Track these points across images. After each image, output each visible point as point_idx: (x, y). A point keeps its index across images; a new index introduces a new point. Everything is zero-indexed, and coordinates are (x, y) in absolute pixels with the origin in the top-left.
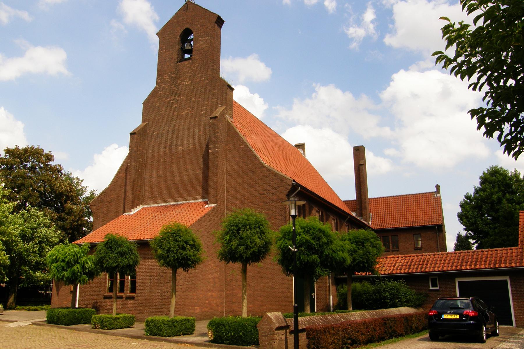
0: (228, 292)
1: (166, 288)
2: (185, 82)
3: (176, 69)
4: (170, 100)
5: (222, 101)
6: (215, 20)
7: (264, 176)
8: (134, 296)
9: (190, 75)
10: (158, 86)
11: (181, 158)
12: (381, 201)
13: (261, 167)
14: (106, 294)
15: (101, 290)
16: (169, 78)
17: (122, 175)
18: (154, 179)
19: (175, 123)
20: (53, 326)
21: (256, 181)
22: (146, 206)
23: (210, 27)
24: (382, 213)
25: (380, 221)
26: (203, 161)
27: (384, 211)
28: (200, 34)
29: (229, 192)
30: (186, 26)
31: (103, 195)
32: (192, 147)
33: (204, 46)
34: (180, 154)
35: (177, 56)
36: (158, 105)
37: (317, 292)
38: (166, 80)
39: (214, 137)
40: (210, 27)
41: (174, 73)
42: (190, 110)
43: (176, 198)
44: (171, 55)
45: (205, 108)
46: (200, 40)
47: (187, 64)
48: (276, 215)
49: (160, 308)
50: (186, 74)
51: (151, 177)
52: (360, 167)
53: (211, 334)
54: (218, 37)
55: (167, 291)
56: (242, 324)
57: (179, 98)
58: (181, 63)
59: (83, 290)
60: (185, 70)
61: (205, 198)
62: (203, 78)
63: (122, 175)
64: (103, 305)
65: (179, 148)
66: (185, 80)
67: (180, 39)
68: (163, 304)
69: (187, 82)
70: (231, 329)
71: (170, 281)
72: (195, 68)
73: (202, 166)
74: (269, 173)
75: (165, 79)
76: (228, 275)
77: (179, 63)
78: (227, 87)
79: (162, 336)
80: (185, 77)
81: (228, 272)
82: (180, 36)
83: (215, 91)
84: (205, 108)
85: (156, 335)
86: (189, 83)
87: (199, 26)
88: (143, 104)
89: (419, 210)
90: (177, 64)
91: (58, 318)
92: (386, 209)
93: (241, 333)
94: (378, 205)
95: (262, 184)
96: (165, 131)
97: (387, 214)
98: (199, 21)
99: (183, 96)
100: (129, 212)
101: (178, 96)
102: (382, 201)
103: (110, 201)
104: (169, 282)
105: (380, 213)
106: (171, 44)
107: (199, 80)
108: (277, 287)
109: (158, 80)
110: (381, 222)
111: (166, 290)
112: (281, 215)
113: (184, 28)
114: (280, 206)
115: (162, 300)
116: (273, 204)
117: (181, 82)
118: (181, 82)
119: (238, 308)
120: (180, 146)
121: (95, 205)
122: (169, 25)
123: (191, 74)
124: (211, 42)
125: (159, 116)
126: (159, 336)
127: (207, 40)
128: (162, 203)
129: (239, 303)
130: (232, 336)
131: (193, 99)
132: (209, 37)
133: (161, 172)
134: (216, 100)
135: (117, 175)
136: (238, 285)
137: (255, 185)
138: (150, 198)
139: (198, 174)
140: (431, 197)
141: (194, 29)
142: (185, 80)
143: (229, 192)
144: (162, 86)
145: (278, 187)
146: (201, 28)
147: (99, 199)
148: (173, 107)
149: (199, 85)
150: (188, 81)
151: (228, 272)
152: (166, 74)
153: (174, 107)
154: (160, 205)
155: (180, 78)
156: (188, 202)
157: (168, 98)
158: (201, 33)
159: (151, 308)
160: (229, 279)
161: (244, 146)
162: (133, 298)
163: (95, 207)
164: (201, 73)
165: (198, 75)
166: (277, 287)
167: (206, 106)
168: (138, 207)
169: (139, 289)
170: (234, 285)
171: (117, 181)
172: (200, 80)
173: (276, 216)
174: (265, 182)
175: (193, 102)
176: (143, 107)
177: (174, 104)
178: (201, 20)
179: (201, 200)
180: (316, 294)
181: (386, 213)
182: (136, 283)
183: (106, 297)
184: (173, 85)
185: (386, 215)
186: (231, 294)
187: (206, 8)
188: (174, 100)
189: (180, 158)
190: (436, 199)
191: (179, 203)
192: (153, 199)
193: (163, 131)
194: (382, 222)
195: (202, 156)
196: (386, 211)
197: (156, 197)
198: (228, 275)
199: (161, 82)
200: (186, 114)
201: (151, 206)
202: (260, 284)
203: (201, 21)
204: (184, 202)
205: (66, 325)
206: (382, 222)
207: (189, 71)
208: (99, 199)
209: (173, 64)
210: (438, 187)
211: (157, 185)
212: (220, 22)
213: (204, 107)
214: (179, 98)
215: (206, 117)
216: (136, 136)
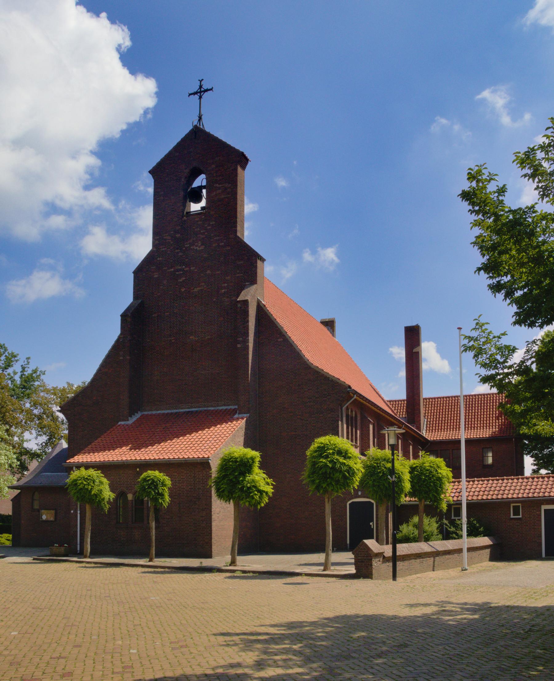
31: (80, 396)
38: (167, 241)
48: (326, 428)
57: (187, 269)
65: (191, 337)
66: (196, 244)
69: (198, 247)
71: (205, 508)
87: (213, 166)
100: (125, 421)
134: (242, 275)
142: (196, 244)
144: (162, 250)
150: (200, 245)
153: (181, 280)
157: (171, 268)
161: (282, 340)
184: (177, 249)
213: (224, 283)
215: (228, 297)
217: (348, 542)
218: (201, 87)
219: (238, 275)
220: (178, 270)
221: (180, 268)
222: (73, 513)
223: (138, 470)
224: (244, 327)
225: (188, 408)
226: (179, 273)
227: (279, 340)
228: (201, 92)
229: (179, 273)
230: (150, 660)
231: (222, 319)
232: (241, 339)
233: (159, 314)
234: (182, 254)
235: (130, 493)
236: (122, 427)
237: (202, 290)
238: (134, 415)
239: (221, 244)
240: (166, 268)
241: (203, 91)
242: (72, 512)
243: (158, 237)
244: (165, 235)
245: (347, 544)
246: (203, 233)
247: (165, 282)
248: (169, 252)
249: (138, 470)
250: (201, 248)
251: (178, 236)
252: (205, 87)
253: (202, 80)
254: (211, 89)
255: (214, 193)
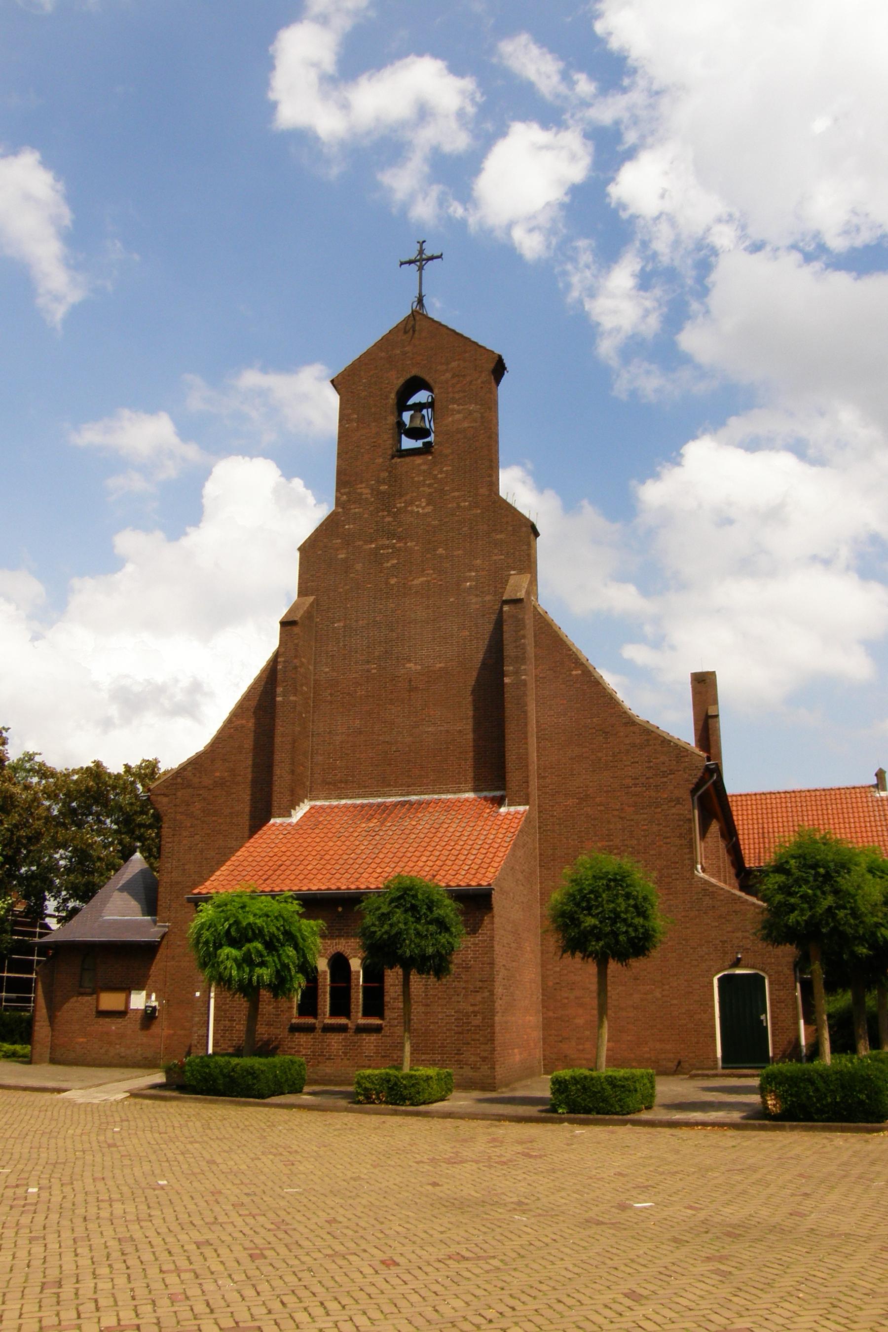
0: (551, 1014)
1: (472, 1005)
2: (417, 506)
3: (390, 472)
4: (377, 548)
5: (520, 561)
6: (491, 366)
7: (634, 745)
8: (381, 1025)
9: (430, 490)
10: (340, 510)
11: (412, 689)
12: (749, 802)
13: (626, 724)
14: (294, 1021)
15: (282, 1011)
16: (372, 494)
17: (244, 722)
18: (338, 738)
19: (393, 605)
20: (217, 1100)
21: (614, 755)
22: (318, 803)
23: (479, 381)
24: (756, 831)
25: (754, 849)
26: (474, 700)
27: (760, 826)
28: (451, 395)
29: (544, 778)
30: (414, 372)
31: (189, 769)
32: (442, 665)
33: (466, 425)
34: (410, 681)
35: (390, 442)
36: (343, 556)
37: (772, 1012)
38: (364, 497)
39: (516, 647)
40: (479, 381)
41: (384, 483)
42: (434, 576)
43: (401, 785)
44: (374, 438)
45: (474, 574)
46: (453, 410)
47: (420, 465)
48: (669, 835)
49: (456, 1054)
50: (418, 488)
51: (330, 733)
52: (710, 721)
53: (774, 1102)
54: (490, 406)
55: (473, 1012)
56: (862, 1076)
57: (402, 545)
58: (403, 459)
59: (225, 1011)
60: (416, 479)
61: (481, 790)
62: (465, 501)
63: (244, 722)
64: (289, 1048)
65: (408, 665)
66: (417, 503)
67: (395, 401)
68: (464, 1044)
69: (422, 508)
70: (832, 1087)
71: (480, 988)
72: (443, 475)
73: (471, 713)
74: (646, 738)
75: (361, 494)
76: (548, 972)
77: (399, 460)
78: (530, 530)
79: (607, 1114)
80: (415, 494)
81: (550, 967)
82: (398, 393)
83: (498, 537)
84: (474, 574)
85: (588, 1111)
86: (429, 509)
87: (448, 375)
88: (299, 549)
89: (842, 825)
90: (393, 461)
91: (232, 1080)
92: (765, 821)
93: (863, 1097)
94: (745, 812)
95: (629, 763)
96: (365, 622)
97: (769, 832)
98: (448, 364)
99: (412, 541)
100: (284, 817)
101: (400, 539)
102: (754, 802)
103: (211, 787)
104: (478, 992)
105: (751, 831)
106: (373, 410)
107: (455, 505)
108: (675, 1002)
109: (339, 495)
110: (757, 851)
111: (471, 1009)
112: (681, 836)
113: (409, 376)
114: (677, 815)
115: (460, 1033)
116: (659, 810)
117: (406, 507)
118: (406, 507)
119: (578, 1050)
120: (410, 661)
121: (165, 795)
122: (366, 364)
123: (432, 490)
124: (482, 417)
125: (346, 584)
126: (598, 1113)
127: (471, 413)
128: (363, 797)
129: (578, 1039)
130: (836, 1102)
131: (441, 551)
132: (476, 404)
133: (358, 722)
134: (503, 557)
135: (229, 722)
136: (576, 998)
137: (612, 764)
138: (329, 783)
139: (460, 731)
140: (866, 797)
141: (435, 382)
142: (417, 503)
143: (544, 778)
144: (353, 511)
145: (671, 770)
146: (455, 381)
147: (179, 780)
148: (385, 565)
149: (456, 518)
150: (424, 504)
151: (550, 967)
152: (361, 483)
153: (389, 565)
154: (358, 802)
155: (401, 496)
156: (436, 796)
157: (371, 542)
158: (454, 393)
159: (429, 1054)
160: (550, 984)
161: (580, 672)
162: (378, 1029)
163: (165, 800)
164: (458, 490)
165: (453, 494)
166: (675, 1002)
167: (477, 571)
168: (301, 804)
169: (394, 1009)
170: (567, 998)
171: (231, 736)
172: (459, 507)
173: (667, 838)
174: (636, 760)
175: (441, 556)
176: (301, 559)
177: (388, 557)
178: (455, 361)
179: (471, 795)
180: (772, 1017)
181: (766, 831)
182: (383, 992)
183: (295, 1029)
184: (383, 510)
185: (766, 835)
186: (557, 1018)
187: (465, 335)
188: (388, 547)
189: (410, 691)
190: (880, 803)
191: (414, 798)
192: (336, 788)
193: (361, 622)
194: (759, 852)
195: (470, 688)
196: (765, 826)
197: (346, 782)
198: (548, 972)
199: (349, 501)
200: (422, 584)
201: (335, 803)
202: (631, 994)
203: (454, 364)
204: (426, 797)
205: (258, 1098)
206: (759, 852)
207: (427, 482)
208: (179, 780)
209: (381, 460)
210: (880, 774)
211: (349, 752)
212: (499, 369)
213: (470, 571)
214: (402, 545)
215: (477, 596)
216: (296, 630)
217: (719, 1054)
218: (421, 252)
219: (495, 558)
220: (384, 547)
221: (387, 542)
222: (199, 997)
223: (340, 909)
224: (516, 647)
225: (402, 795)
226: (385, 551)
227: (574, 673)
228: (421, 260)
229: (385, 551)
230: (264, 1303)
231: (468, 633)
232: (512, 668)
233: (348, 622)
234: (390, 519)
235: (355, 957)
236: (281, 828)
237: (428, 582)
238: (295, 809)
239: (462, 504)
240: (361, 543)
241: (424, 260)
242: (198, 994)
243: (347, 490)
244: (360, 486)
245: (717, 1058)
246: (430, 486)
247: (359, 566)
248: (366, 516)
249: (340, 909)
250: (426, 510)
251: (384, 488)
252: (428, 253)
253: (424, 242)
254: (440, 257)
255: (450, 419)
